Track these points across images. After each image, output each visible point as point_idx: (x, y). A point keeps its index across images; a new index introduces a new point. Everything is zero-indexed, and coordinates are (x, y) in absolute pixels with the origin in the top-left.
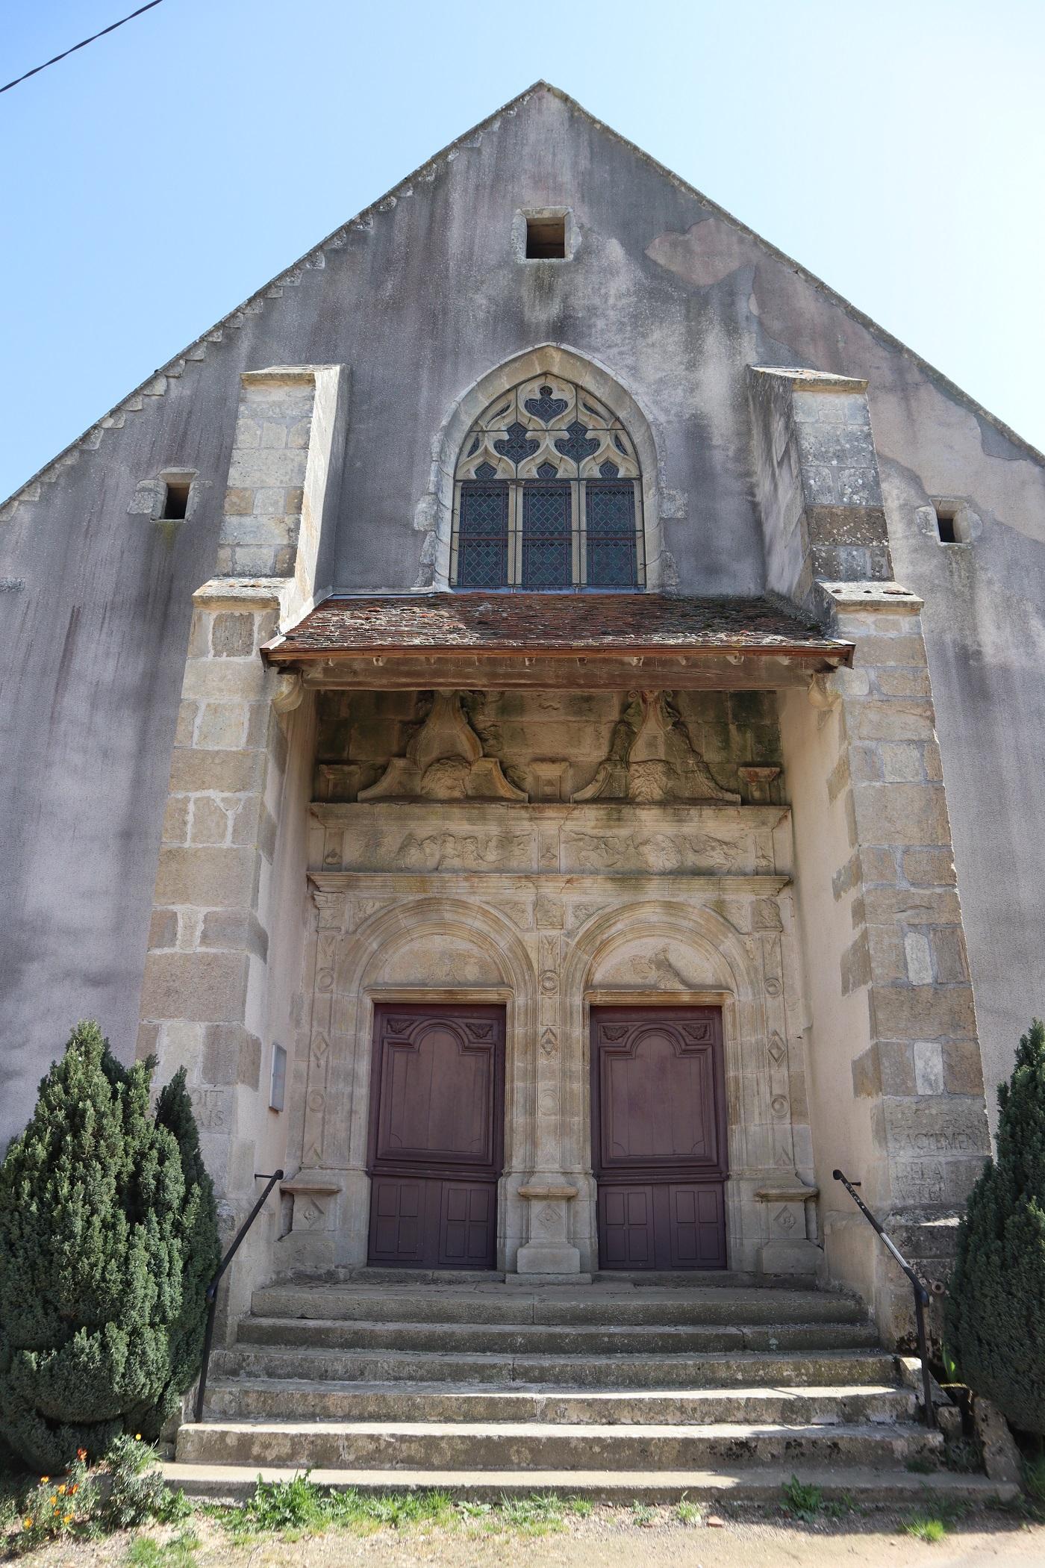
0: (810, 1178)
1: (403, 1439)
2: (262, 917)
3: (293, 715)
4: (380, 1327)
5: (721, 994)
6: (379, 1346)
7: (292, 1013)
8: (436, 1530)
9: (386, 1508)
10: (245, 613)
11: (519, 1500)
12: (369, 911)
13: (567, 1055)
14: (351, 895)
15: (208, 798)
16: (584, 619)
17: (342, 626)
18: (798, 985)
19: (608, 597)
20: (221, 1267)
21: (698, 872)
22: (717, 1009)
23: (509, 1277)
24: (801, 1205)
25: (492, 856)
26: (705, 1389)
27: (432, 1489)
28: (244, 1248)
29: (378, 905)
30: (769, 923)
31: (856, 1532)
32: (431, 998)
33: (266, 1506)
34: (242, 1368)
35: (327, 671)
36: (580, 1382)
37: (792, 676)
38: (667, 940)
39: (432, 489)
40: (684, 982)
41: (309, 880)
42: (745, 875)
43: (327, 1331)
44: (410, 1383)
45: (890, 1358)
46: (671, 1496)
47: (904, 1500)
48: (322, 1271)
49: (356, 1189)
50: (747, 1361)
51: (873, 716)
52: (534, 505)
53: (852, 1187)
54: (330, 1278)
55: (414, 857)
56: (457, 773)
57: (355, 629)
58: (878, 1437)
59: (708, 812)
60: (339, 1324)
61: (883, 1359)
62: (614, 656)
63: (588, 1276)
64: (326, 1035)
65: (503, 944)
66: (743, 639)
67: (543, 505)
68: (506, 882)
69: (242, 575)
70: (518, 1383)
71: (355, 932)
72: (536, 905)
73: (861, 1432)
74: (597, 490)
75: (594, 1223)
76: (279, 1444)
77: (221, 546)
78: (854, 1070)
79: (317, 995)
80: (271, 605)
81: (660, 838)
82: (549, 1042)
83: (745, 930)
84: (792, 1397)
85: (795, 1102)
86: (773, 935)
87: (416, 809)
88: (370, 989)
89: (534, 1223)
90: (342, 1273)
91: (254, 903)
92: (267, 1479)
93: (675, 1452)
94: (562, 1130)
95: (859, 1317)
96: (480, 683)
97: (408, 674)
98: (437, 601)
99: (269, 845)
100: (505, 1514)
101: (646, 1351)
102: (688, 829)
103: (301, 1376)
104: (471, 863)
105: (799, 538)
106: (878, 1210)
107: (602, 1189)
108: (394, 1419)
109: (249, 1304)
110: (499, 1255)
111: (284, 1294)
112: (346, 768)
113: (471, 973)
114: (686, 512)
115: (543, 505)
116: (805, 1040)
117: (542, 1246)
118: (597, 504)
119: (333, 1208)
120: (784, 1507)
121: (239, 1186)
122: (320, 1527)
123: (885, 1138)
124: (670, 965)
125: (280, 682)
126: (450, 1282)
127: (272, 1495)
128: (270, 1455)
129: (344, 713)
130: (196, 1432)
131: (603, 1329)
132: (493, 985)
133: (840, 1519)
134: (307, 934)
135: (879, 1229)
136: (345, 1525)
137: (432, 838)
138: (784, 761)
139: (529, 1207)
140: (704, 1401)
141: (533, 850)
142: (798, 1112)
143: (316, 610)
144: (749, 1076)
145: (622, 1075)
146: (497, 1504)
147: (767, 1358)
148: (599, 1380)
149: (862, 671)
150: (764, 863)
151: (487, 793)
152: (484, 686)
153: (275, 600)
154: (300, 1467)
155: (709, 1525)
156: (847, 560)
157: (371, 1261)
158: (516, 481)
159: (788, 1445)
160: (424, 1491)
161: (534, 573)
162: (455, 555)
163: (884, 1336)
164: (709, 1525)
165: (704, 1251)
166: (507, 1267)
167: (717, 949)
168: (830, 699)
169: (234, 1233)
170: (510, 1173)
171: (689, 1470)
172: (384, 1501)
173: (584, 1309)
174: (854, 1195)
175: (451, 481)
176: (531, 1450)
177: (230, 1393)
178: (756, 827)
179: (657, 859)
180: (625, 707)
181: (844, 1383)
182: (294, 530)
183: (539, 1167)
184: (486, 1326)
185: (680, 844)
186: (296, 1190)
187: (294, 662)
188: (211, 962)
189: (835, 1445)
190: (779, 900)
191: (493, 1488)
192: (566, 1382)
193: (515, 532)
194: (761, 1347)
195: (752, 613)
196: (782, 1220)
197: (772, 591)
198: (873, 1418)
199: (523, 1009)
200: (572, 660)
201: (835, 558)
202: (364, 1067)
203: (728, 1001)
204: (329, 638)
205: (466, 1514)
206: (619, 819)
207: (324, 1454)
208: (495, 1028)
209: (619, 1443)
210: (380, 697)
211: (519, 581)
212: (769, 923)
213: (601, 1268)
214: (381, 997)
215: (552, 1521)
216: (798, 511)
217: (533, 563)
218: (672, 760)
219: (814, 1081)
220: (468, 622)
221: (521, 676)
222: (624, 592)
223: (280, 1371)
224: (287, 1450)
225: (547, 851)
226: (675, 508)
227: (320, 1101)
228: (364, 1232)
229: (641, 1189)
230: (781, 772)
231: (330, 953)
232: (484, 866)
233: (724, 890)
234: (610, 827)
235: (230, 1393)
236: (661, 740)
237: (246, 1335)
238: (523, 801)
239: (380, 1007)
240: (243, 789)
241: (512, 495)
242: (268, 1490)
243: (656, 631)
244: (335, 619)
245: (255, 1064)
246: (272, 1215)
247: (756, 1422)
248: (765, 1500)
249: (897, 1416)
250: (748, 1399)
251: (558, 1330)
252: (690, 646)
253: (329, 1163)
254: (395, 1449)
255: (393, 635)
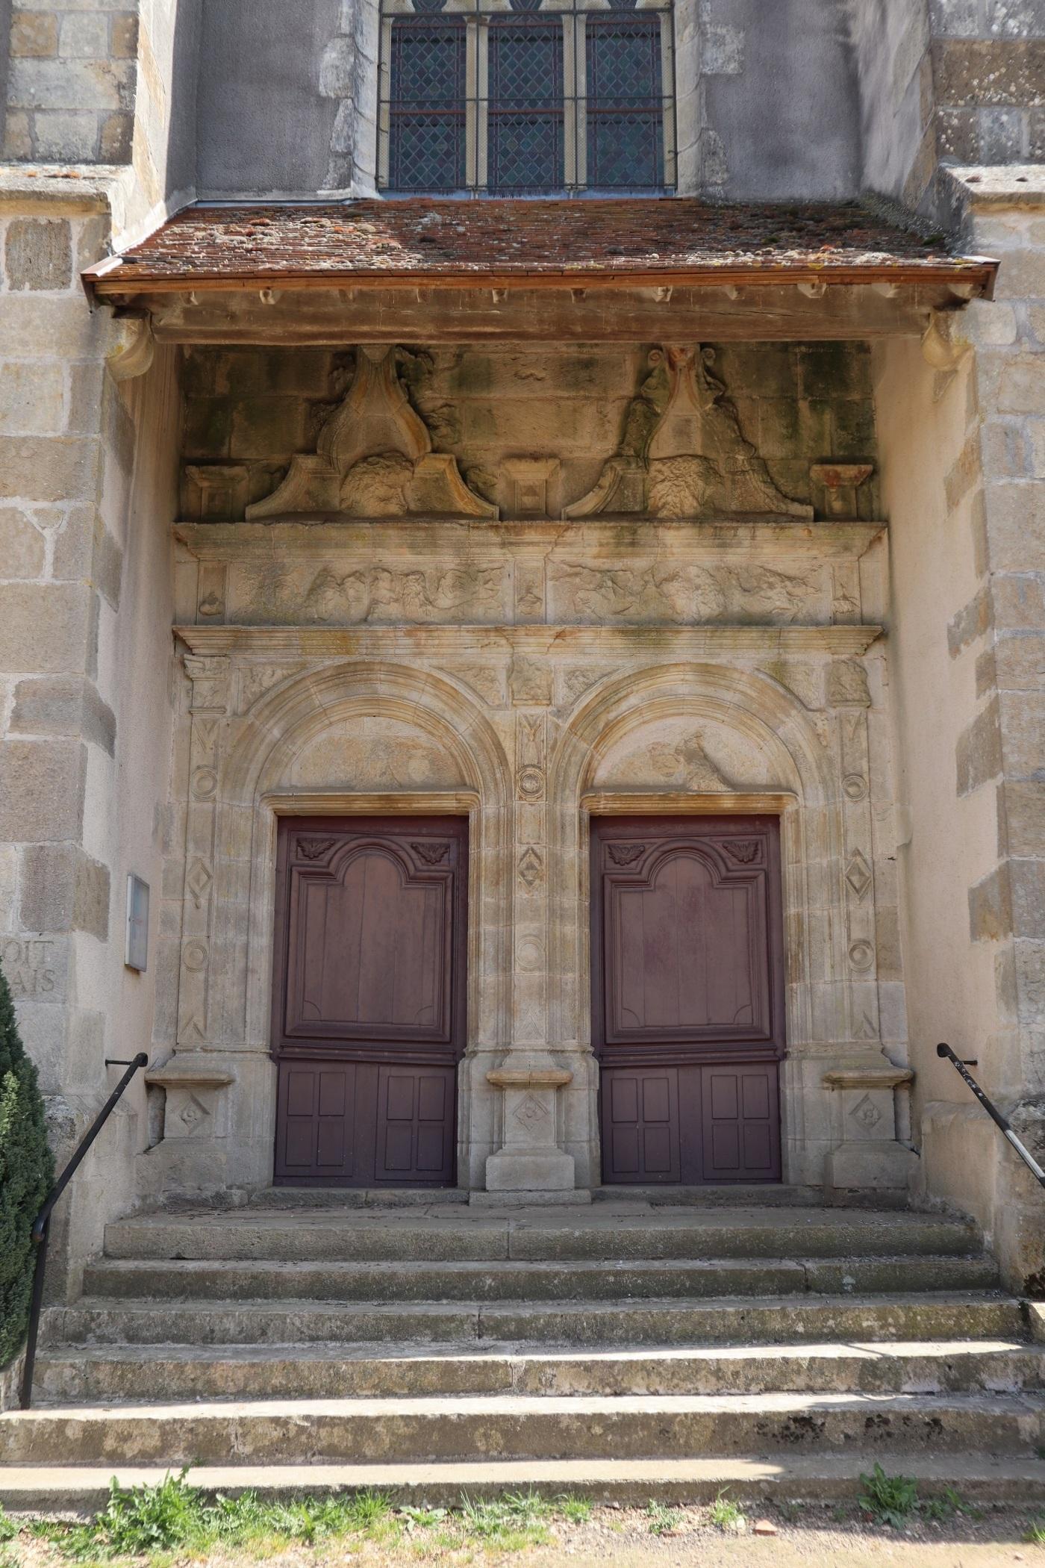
0: (903, 1056)
1: (321, 1421)
2: (104, 688)
3: (140, 384)
4: (289, 1269)
5: (779, 798)
6: (288, 1294)
7: (155, 831)
8: (368, 1546)
9: (295, 1518)
10: (57, 220)
11: (487, 1502)
12: (267, 682)
13: (557, 886)
14: (240, 659)
15: (14, 510)
16: (583, 234)
17: (211, 245)
18: (891, 783)
19: (619, 203)
20: (54, 1192)
21: (748, 621)
22: (773, 820)
23: (474, 1196)
24: (890, 1093)
25: (446, 600)
26: (752, 1345)
27: (363, 1490)
28: (90, 1163)
29: (279, 673)
30: (852, 695)
31: (966, 1540)
32: (360, 807)
33: (124, 1522)
34: (89, 1330)
35: (189, 314)
36: (574, 1338)
37: (899, 318)
38: (702, 721)
39: (345, 27)
40: (725, 780)
41: (177, 638)
42: (818, 624)
43: (214, 1276)
44: (332, 1344)
45: (1015, 1303)
46: (705, 1493)
47: (1033, 1497)
48: (208, 1194)
49: (256, 1080)
50: (811, 1306)
51: (1020, 377)
52: (505, 57)
53: (964, 1067)
54: (220, 1203)
55: (331, 602)
56: (393, 478)
57: (229, 249)
58: (997, 1411)
59: (764, 532)
60: (230, 1265)
61: (1005, 1304)
62: (627, 287)
63: (585, 1194)
64: (207, 861)
65: (464, 727)
66: (826, 257)
67: (519, 57)
68: (467, 638)
69: (48, 159)
70: (486, 1341)
71: (246, 713)
72: (511, 670)
73: (973, 1404)
74: (602, 31)
75: (595, 1121)
76: (142, 1435)
77: (12, 110)
78: (972, 901)
79: (193, 805)
80: (97, 205)
81: (693, 571)
82: (530, 867)
83: (815, 705)
84: (874, 1356)
85: (883, 951)
86: (856, 711)
87: (332, 531)
88: (270, 796)
89: (510, 1121)
90: (237, 1196)
91: (91, 668)
92: (124, 1484)
93: (708, 1433)
94: (550, 991)
95: (969, 1246)
96: (424, 333)
97: (314, 319)
98: (358, 210)
99: (111, 580)
100: (466, 1523)
101: (667, 1294)
102: (735, 557)
103: (176, 1339)
104: (415, 610)
105: (917, 97)
106: (1002, 1099)
107: (606, 1073)
108: (310, 1395)
109: (99, 1242)
110: (460, 1167)
111: (151, 1225)
112: (227, 471)
113: (418, 770)
114: (742, 64)
115: (519, 57)
116: (899, 863)
117: (521, 1152)
118: (603, 55)
119: (223, 1106)
120: (864, 1505)
121: (82, 1077)
122: (201, 1548)
123: (1016, 998)
124: (706, 757)
125: (117, 331)
126: (391, 1205)
127: (132, 1506)
128: (130, 1449)
129: (222, 387)
130: (22, 1421)
131: (607, 1265)
132: (449, 788)
133: (943, 1523)
134: (176, 717)
135: (1003, 1125)
136: (237, 1544)
137: (358, 575)
138: (881, 457)
139: (502, 1099)
140: (750, 1363)
141: (507, 591)
142: (886, 965)
143: (170, 223)
144: (821, 919)
145: (635, 913)
146: (456, 1509)
147: (840, 1303)
148: (601, 1336)
149: (1005, 307)
150: (845, 606)
151: (439, 507)
152: (431, 337)
153: (102, 198)
154: (174, 1464)
155: (756, 1532)
156: (991, 131)
157: (279, 1177)
158: (477, 16)
159: (869, 1423)
160: (351, 1493)
161: (505, 169)
162: (385, 140)
163: (1007, 1273)
164: (756, 1532)
165: (752, 1158)
166: (472, 1183)
167: (773, 731)
168: (955, 352)
169: (75, 1144)
170: (475, 1053)
171: (728, 1456)
172: (294, 1508)
173: (580, 1238)
174: (968, 1078)
175: (376, 16)
176: (505, 1433)
177: (72, 1366)
178: (835, 555)
179: (688, 603)
180: (643, 376)
181: (948, 1337)
182: (127, 87)
183: (519, 1043)
184: (440, 1264)
185: (723, 579)
186: (168, 1082)
187: (140, 298)
188: (27, 755)
189: (936, 1422)
190: (865, 661)
191: (450, 1487)
192: (555, 1338)
193: (477, 100)
194: (832, 1288)
195: (839, 222)
196: (861, 1114)
197: (870, 190)
198: (991, 1385)
199: (493, 822)
200: (562, 296)
201: (972, 127)
202: (264, 908)
203: (789, 808)
204: (189, 261)
205: (412, 1523)
206: (633, 544)
207: (209, 1446)
208: (453, 848)
209: (628, 1422)
210: (276, 360)
211: (483, 180)
212: (852, 695)
213: (604, 1182)
214: (287, 807)
215: (533, 1530)
216: (918, 51)
217: (505, 153)
218: (713, 455)
219: (911, 920)
220: (404, 239)
221: (487, 320)
222: (644, 196)
223: (146, 1334)
224: (154, 1441)
225: (527, 592)
226: (723, 59)
227: (201, 955)
228: (269, 1138)
229: (661, 1073)
230: (875, 472)
231: (209, 744)
232: (434, 615)
233: (786, 646)
234: (620, 556)
235: (72, 1366)
236: (696, 425)
237: (95, 1284)
238: (491, 518)
239: (286, 822)
240: (67, 495)
241: (471, 38)
242: (126, 1499)
243: (691, 249)
244: (200, 234)
245: (102, 903)
246: (132, 1118)
247: (823, 1390)
248: (837, 1498)
249: (1024, 1383)
250: (813, 1359)
251: (543, 1267)
252: (744, 268)
253: (217, 1042)
254: (310, 1436)
255: (291, 257)
